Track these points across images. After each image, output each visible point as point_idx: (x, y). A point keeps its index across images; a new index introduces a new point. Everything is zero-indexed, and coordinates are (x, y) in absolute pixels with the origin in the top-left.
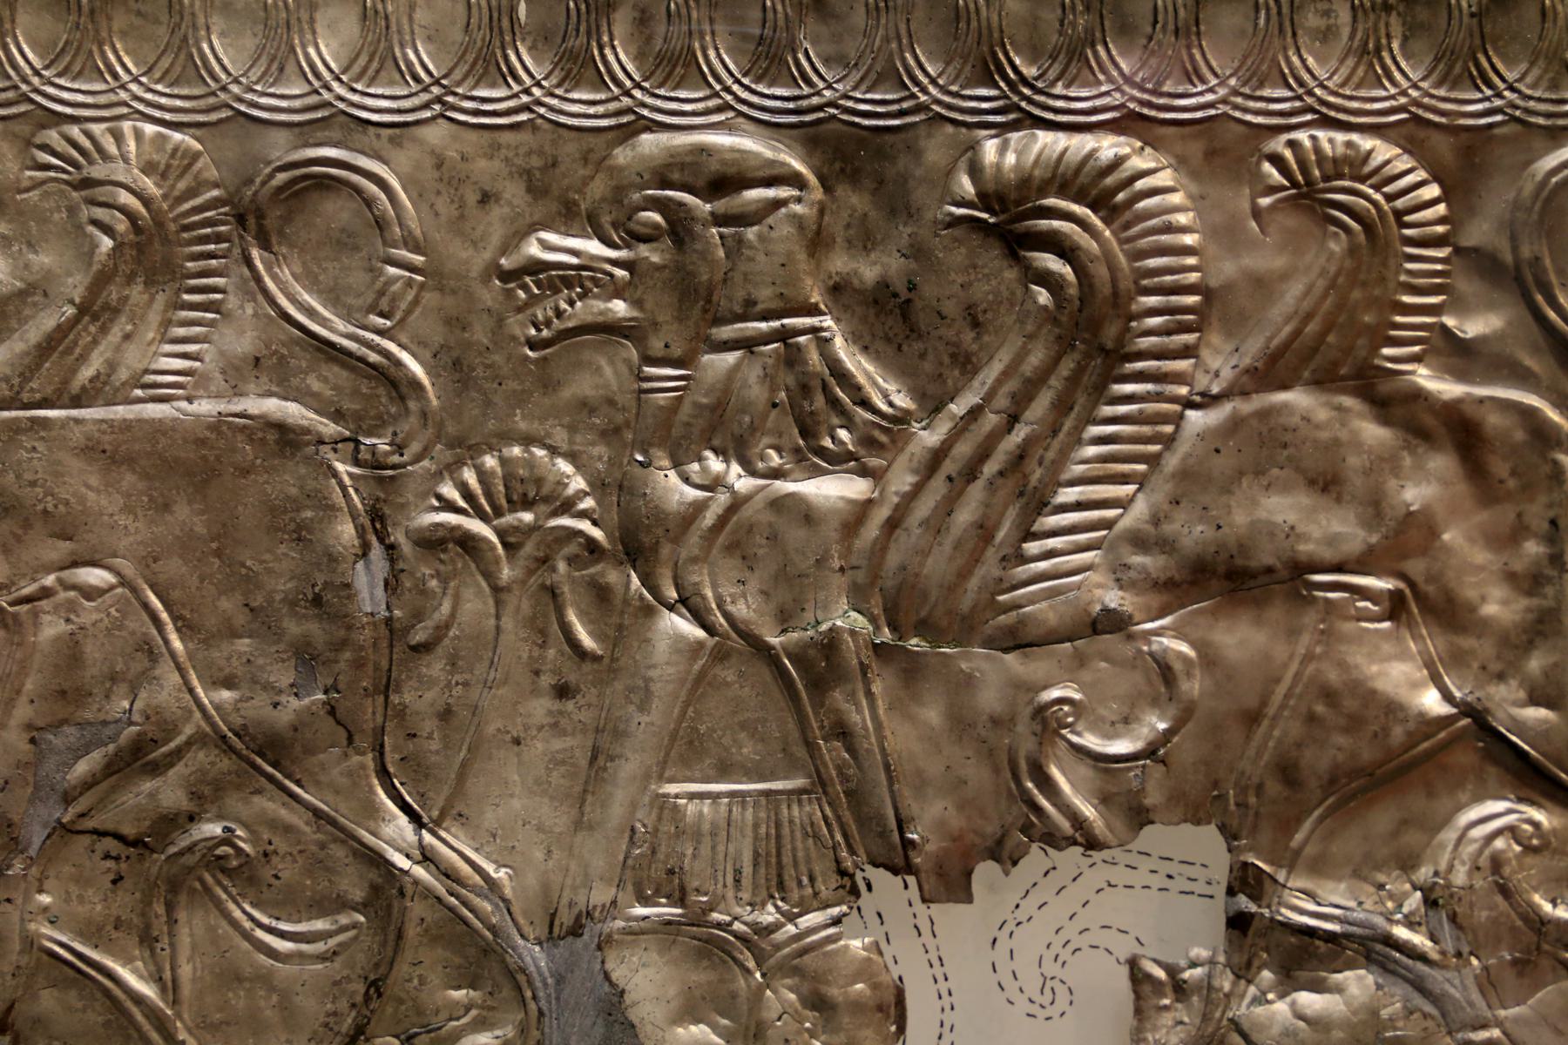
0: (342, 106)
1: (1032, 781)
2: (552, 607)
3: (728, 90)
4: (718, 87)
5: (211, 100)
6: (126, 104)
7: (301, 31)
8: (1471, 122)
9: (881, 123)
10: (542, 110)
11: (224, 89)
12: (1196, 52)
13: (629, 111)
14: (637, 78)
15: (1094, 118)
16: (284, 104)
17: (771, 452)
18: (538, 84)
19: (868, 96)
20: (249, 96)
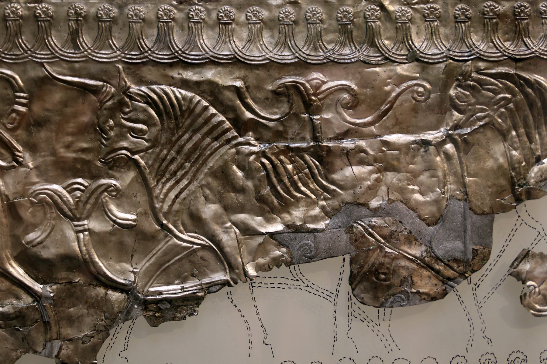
0: (90, 56)
1: (515, 91)
2: (395, 105)
3: (57, 52)
4: (174, 51)
5: (82, 54)
6: (58, 57)
7: (199, 35)
8: (7, 61)
9: (135, 61)
10: (151, 58)
11: (86, 51)
12: (141, 41)
13: (146, 57)
14: (89, 46)
15: (461, 59)
16: (105, 56)
17: (330, 103)
18: (89, 49)
19: (42, 52)
20: (184, 55)
